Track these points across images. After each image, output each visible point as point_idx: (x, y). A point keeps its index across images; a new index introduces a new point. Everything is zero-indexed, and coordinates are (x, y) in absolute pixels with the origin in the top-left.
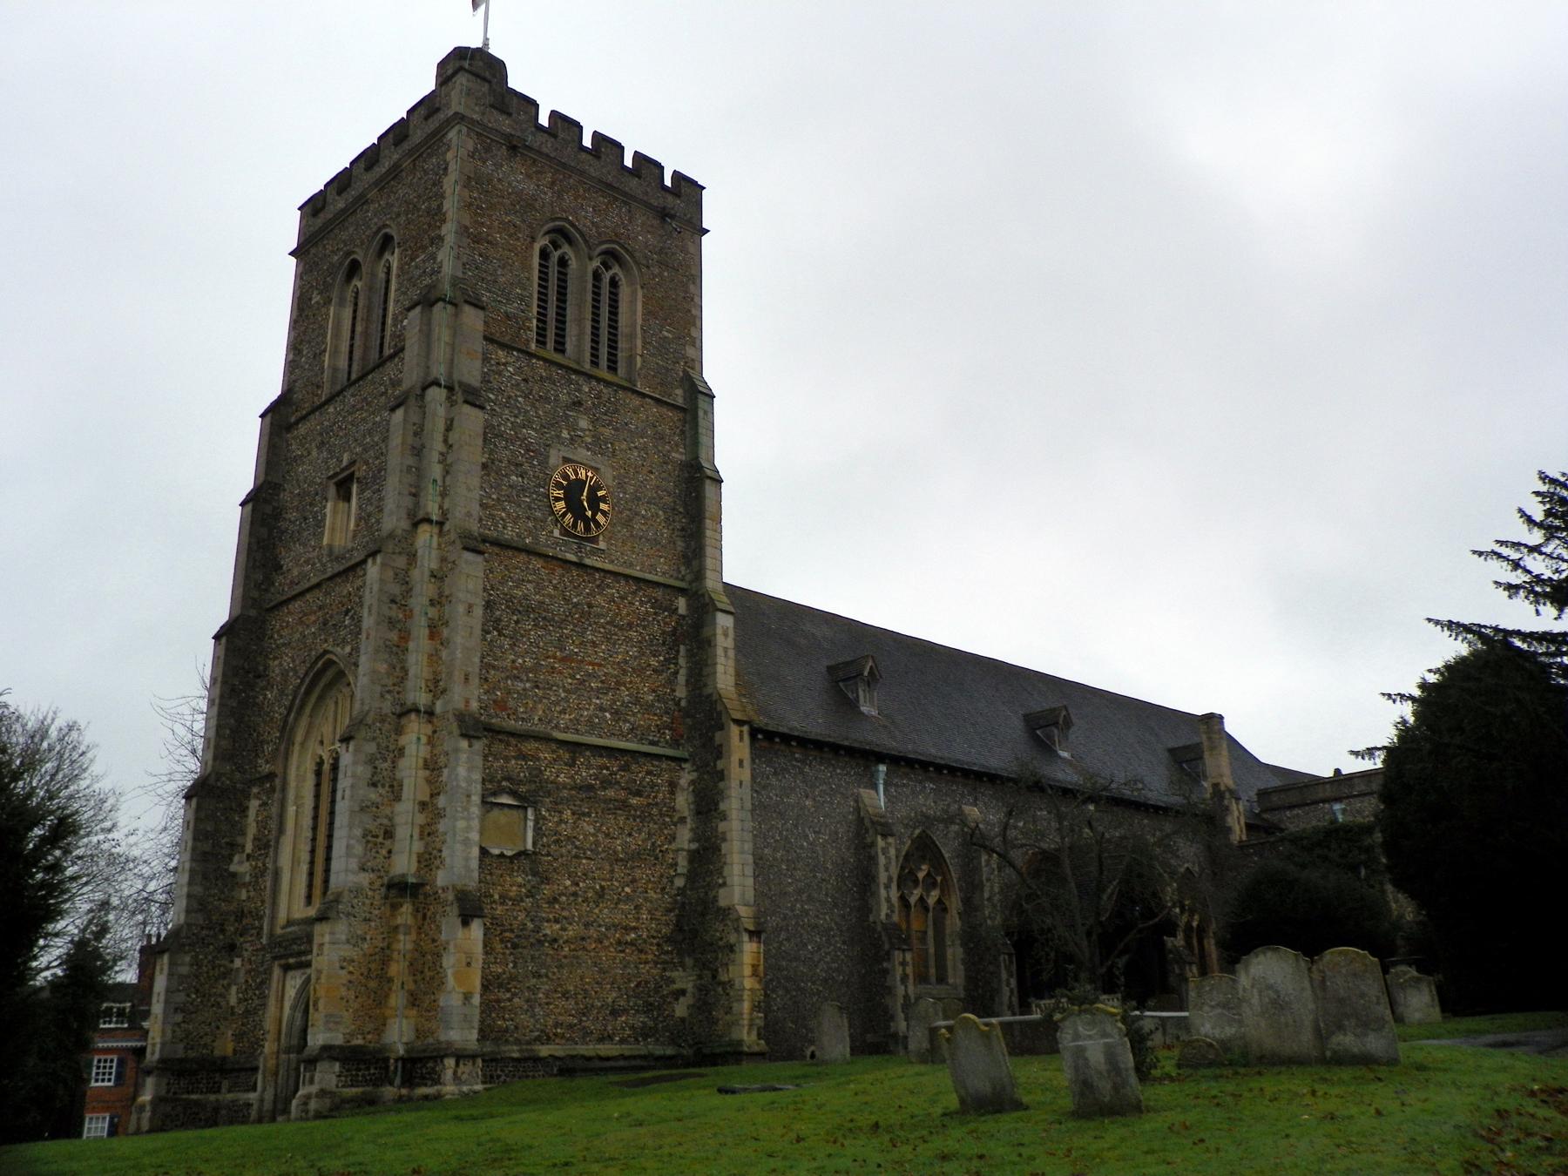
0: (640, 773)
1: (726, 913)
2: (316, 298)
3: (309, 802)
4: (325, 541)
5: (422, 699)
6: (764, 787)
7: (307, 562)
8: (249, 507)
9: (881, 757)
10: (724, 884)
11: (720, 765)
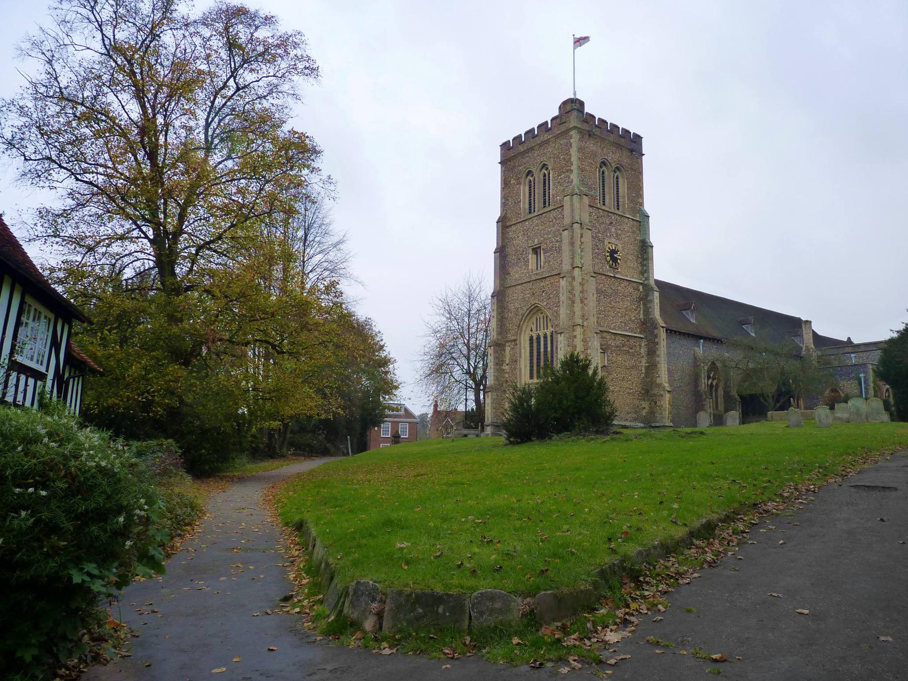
0: (632, 341)
1: (659, 385)
3: (528, 349)
5: (580, 321)
9: (701, 338)
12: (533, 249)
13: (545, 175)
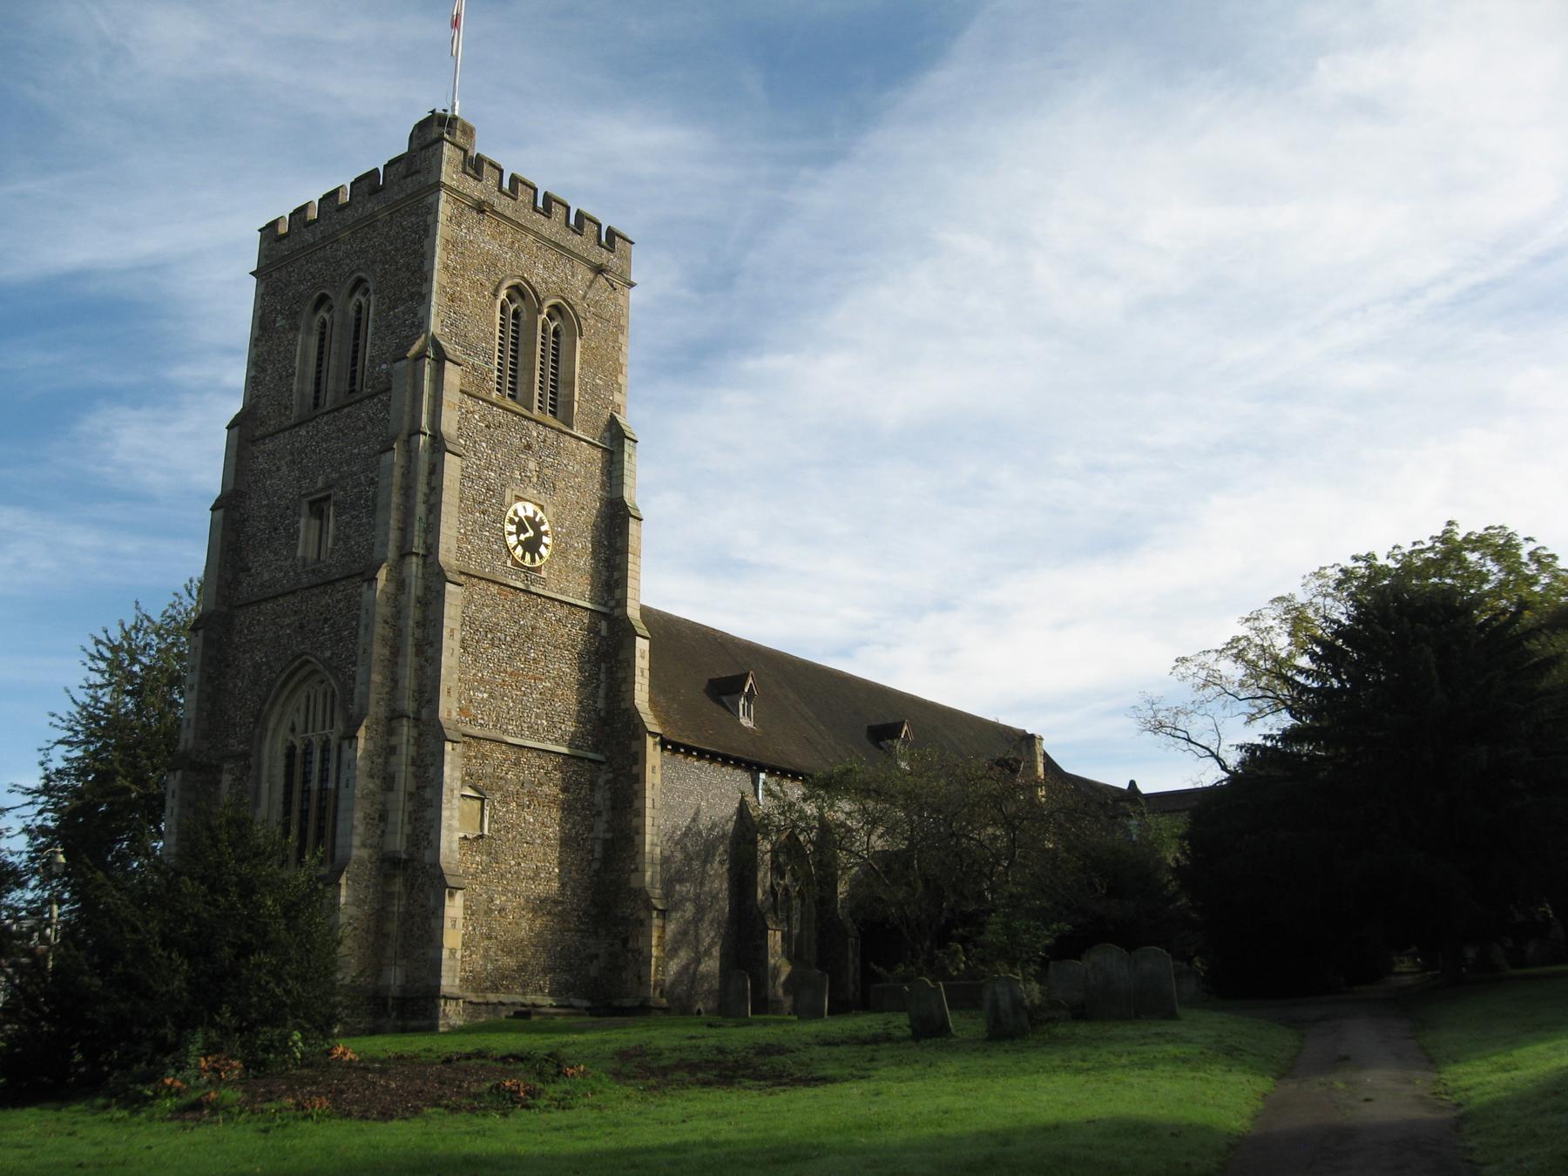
2: (281, 322)
3: (280, 781)
4: (299, 553)
6: (670, 790)
7: (280, 569)
8: (220, 513)
10: (636, 870)
11: (635, 770)
12: (311, 503)
13: (359, 308)
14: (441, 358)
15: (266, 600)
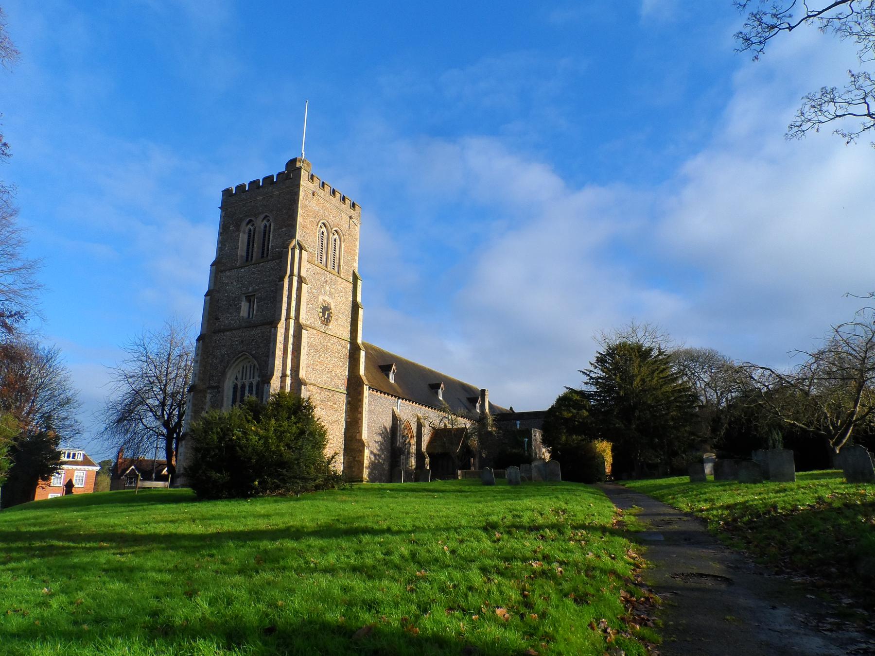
8: (208, 298)
13: (266, 226)
14: (301, 248)
15: (227, 331)
